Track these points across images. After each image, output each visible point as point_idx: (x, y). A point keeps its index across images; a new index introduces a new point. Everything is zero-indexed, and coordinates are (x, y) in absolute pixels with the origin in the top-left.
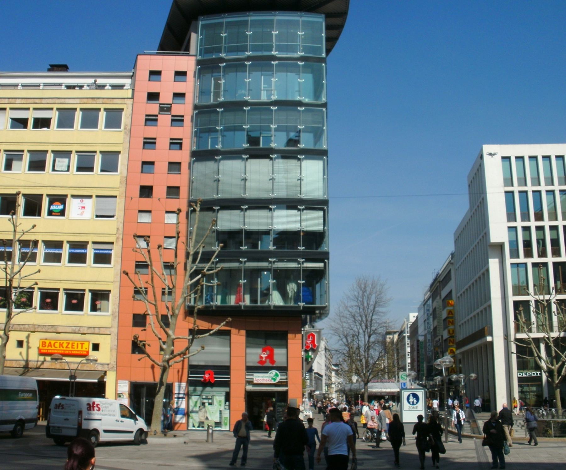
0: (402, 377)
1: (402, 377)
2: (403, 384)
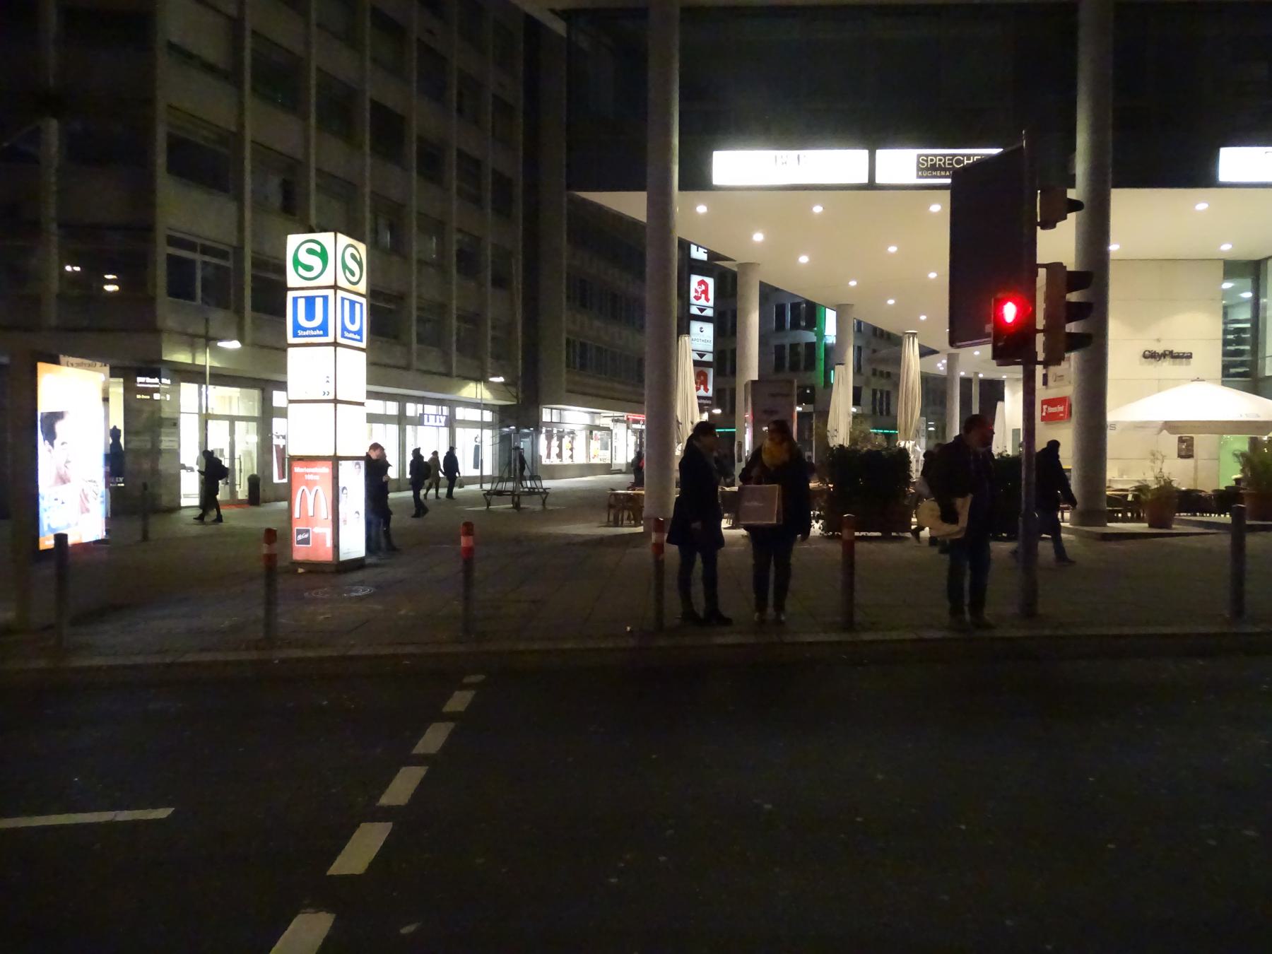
0: (297, 262)
2: (301, 303)
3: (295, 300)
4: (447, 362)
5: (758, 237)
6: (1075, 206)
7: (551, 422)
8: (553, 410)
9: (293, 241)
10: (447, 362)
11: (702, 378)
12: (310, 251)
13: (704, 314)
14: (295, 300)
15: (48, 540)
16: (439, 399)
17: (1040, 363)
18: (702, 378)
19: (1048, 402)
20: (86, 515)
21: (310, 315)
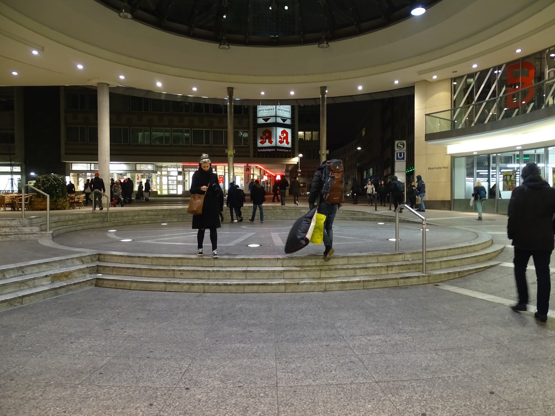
0: (398, 146)
1: (398, 146)
2: (399, 154)
3: (397, 153)
4: (381, 204)
5: (360, 88)
6: (202, 193)
7: (91, 170)
8: (91, 164)
9: (396, 142)
10: (381, 204)
11: (267, 135)
12: (400, 144)
13: (269, 121)
14: (397, 153)
15: (207, 233)
16: (79, 248)
17: (247, 165)
18: (267, 135)
19: (172, 183)
20: (480, 221)
21: (400, 156)
